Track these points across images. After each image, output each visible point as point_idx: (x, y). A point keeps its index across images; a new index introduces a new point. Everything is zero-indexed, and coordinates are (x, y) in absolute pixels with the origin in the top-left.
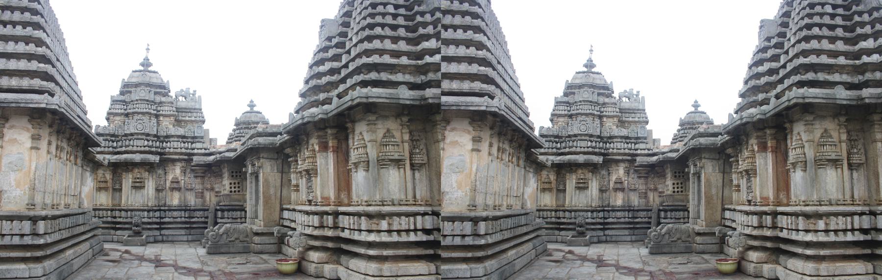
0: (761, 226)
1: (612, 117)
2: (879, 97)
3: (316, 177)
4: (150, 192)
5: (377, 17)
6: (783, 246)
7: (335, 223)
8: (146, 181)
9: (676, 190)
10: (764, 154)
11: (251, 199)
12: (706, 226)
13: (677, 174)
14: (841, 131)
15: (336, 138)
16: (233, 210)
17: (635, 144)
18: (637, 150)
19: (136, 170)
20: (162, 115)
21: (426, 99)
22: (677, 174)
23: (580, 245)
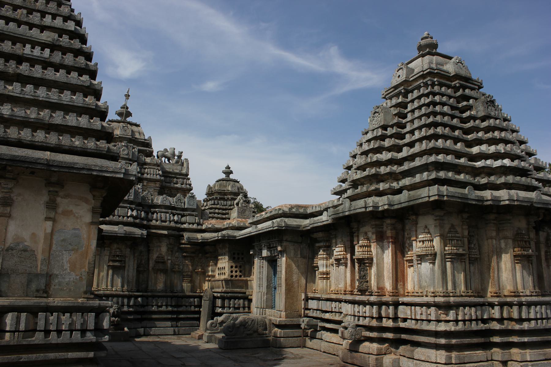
0: (380, 318)
1: (155, 181)
2: (547, 203)
3: (371, 269)
4: (131, 274)
5: (11, 24)
6: (404, 336)
7: (396, 313)
8: (127, 259)
9: (234, 274)
10: (380, 243)
11: (260, 286)
12: (287, 317)
13: (236, 256)
14: (464, 227)
15: (394, 228)
16: (235, 298)
17: (183, 216)
18: (183, 223)
19: (115, 246)
20: (146, 179)
21: (483, 201)
22: (236, 256)
23: (120, 341)
